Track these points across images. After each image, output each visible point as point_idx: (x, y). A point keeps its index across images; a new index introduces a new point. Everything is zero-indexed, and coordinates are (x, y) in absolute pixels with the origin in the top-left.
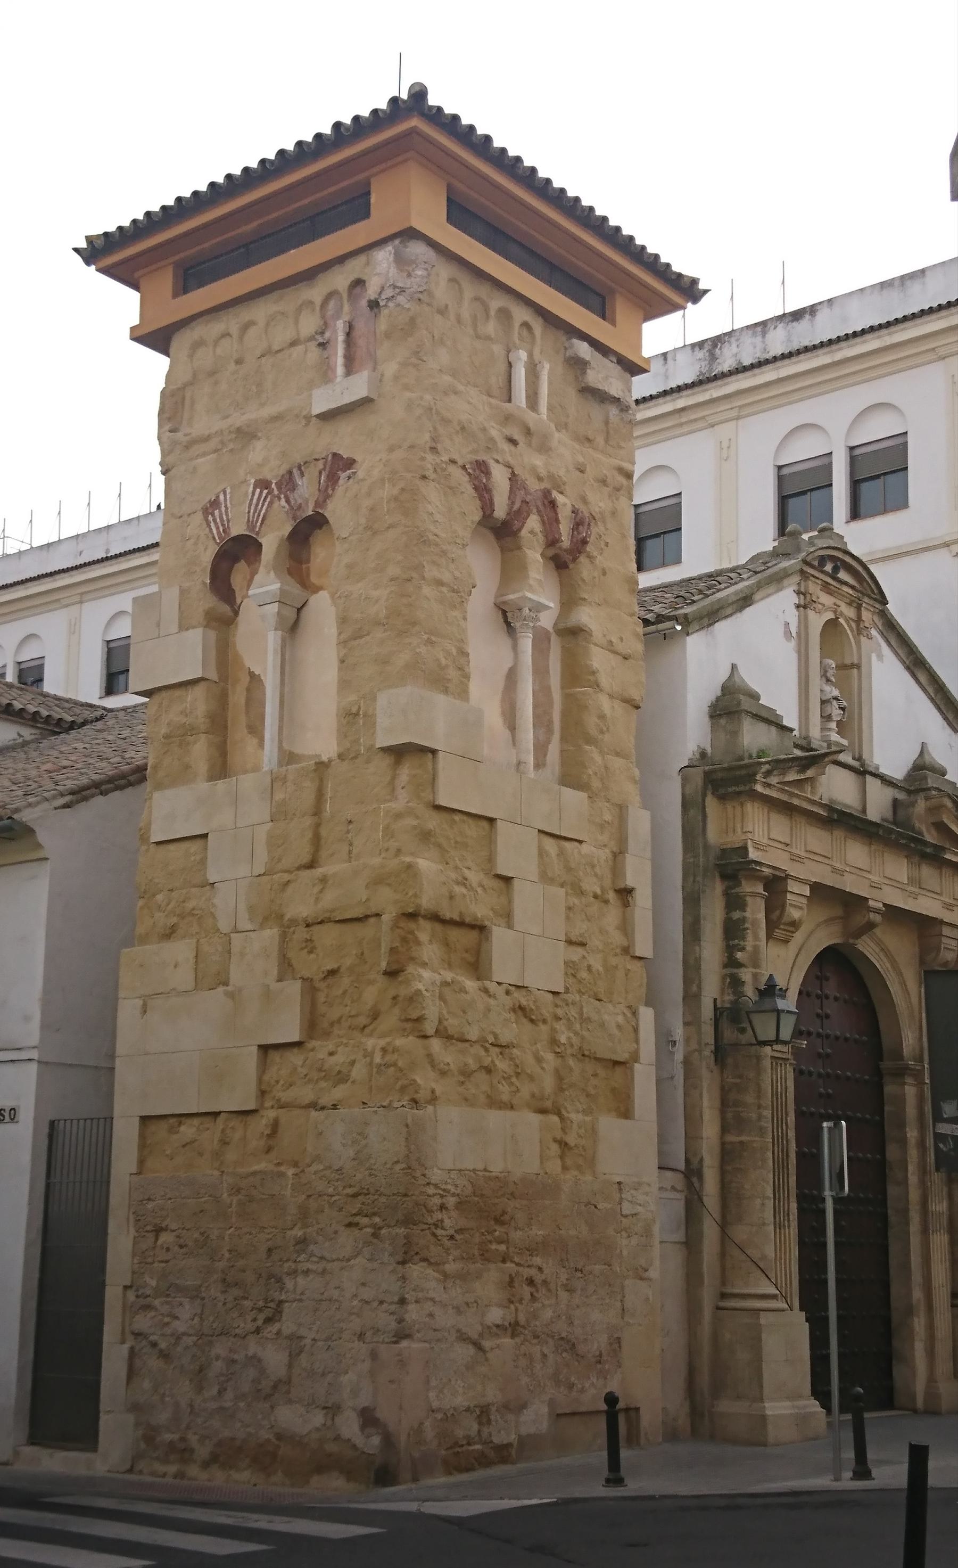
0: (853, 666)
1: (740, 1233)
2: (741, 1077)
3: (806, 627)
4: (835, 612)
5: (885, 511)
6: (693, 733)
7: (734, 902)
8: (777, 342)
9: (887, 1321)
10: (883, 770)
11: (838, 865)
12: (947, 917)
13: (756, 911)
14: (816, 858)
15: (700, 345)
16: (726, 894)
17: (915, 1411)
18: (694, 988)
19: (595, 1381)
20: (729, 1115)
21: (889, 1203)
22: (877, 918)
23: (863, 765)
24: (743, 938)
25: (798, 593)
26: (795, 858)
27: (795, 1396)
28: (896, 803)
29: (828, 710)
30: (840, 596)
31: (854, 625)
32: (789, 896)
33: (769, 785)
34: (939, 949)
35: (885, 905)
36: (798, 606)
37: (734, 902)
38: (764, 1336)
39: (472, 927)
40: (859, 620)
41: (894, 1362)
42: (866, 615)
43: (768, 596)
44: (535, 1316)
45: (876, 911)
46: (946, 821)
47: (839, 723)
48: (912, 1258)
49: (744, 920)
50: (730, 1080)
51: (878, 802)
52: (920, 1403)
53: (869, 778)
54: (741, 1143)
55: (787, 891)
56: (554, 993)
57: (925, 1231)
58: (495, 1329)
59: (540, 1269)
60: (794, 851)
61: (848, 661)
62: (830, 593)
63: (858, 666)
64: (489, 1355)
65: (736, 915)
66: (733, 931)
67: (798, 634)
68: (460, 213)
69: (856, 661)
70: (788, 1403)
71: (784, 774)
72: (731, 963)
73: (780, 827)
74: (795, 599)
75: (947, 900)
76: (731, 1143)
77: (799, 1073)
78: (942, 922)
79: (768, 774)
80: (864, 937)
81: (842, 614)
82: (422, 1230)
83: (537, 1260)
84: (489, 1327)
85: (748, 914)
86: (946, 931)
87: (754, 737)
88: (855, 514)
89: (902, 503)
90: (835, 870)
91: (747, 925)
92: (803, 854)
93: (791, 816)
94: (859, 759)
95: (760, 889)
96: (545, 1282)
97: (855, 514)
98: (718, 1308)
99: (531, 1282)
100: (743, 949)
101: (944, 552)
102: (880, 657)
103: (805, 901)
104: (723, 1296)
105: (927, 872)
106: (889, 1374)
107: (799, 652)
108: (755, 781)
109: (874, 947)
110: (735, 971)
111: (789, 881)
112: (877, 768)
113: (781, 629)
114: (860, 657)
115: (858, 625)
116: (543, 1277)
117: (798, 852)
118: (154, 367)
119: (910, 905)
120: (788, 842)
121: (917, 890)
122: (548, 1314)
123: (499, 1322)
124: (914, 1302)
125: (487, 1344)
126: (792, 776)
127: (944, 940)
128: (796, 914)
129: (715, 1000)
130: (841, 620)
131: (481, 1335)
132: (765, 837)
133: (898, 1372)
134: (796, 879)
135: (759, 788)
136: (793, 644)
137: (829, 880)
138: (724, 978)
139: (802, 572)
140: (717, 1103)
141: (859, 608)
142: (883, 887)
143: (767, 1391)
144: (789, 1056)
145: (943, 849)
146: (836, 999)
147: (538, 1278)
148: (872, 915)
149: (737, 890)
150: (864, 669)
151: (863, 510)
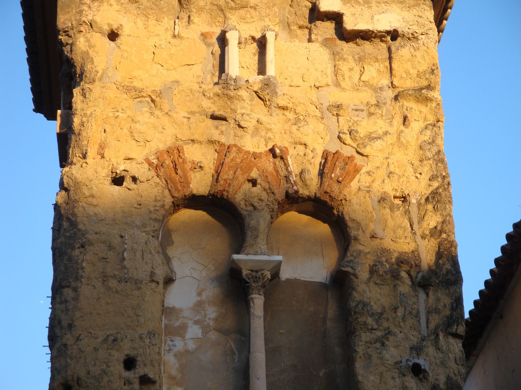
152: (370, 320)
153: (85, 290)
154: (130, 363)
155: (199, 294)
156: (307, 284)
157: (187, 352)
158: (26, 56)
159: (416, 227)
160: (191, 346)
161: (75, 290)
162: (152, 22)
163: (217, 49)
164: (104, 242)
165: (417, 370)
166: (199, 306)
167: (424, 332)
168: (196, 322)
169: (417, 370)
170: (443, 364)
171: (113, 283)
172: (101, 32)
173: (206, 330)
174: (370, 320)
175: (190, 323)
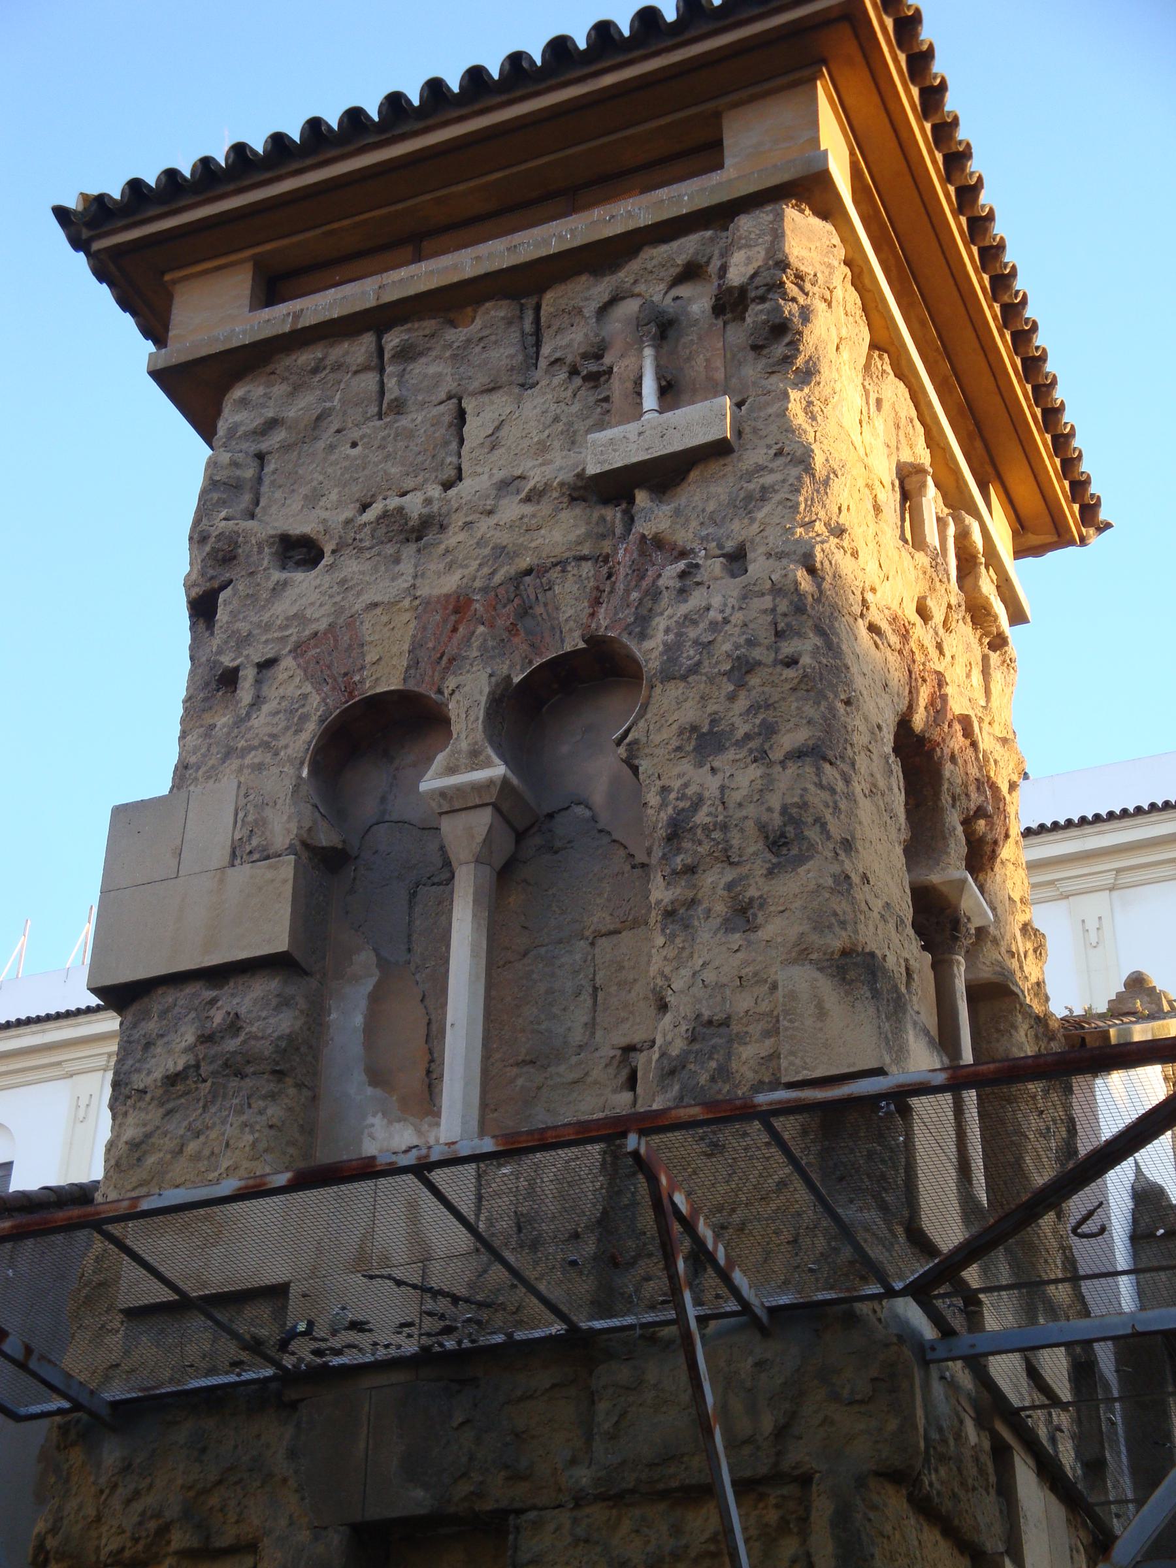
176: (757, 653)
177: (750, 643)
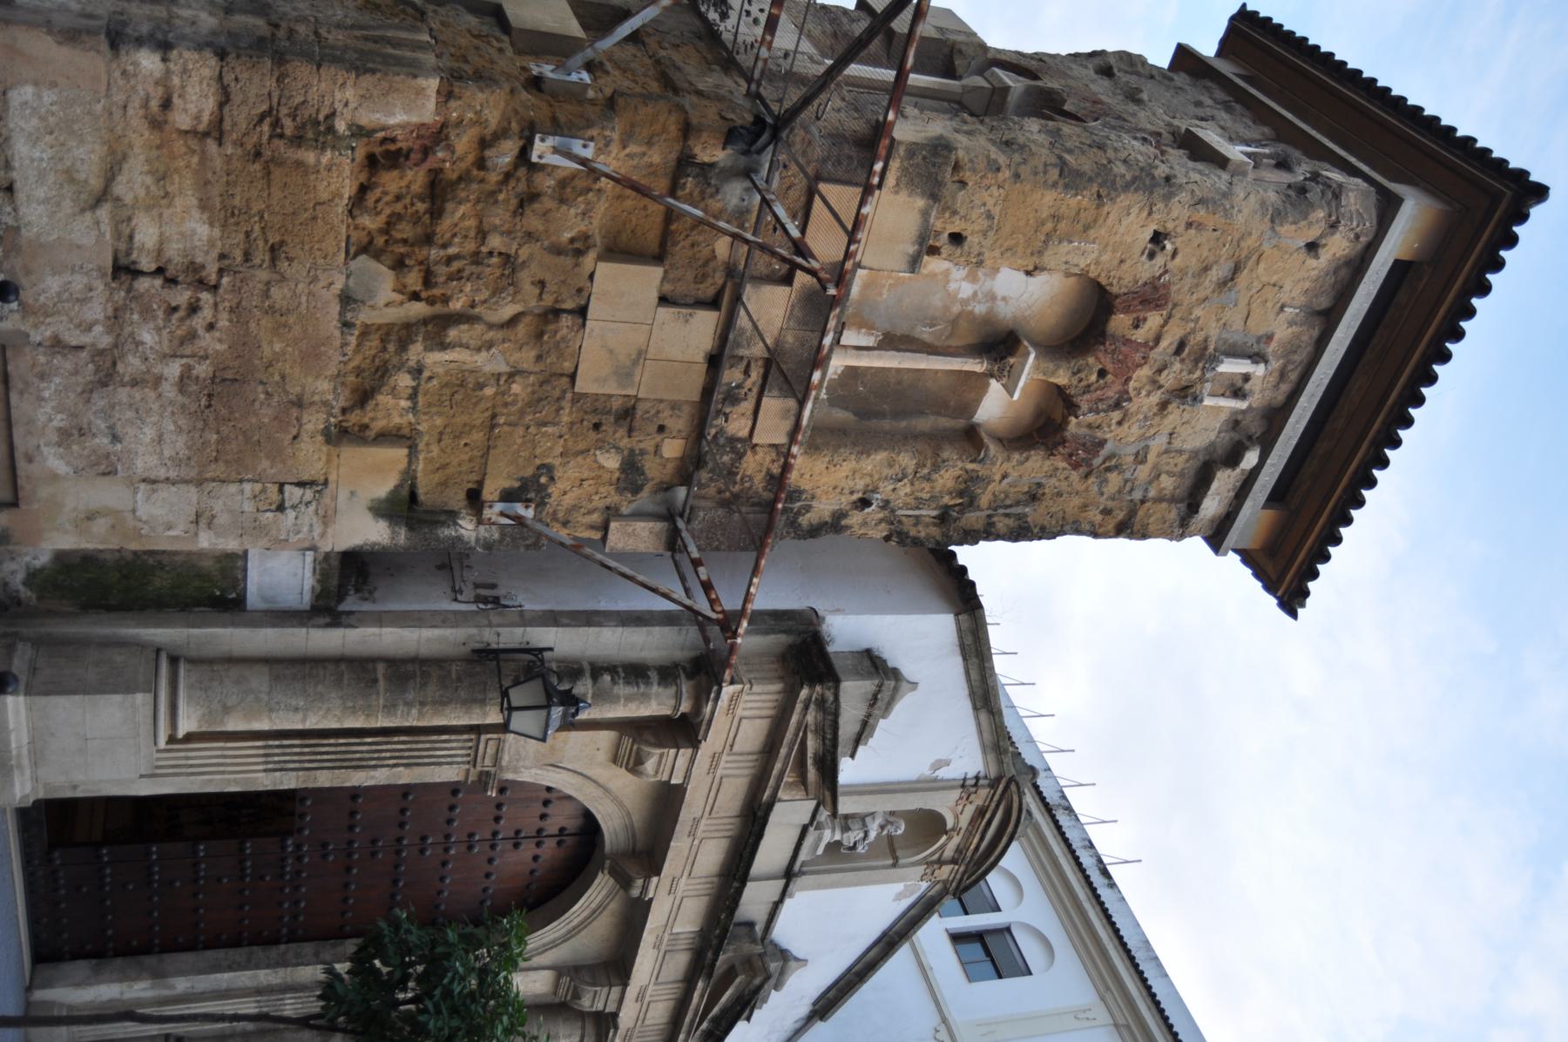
0: (896, 859)
1: (259, 680)
2: (459, 679)
3: (943, 788)
4: (953, 829)
5: (963, 964)
6: (847, 629)
7: (667, 674)
8: (1087, 860)
9: (146, 950)
10: (788, 902)
11: (702, 827)
12: (632, 991)
13: (657, 703)
14: (712, 794)
15: (1064, 797)
16: (676, 665)
17: (29, 989)
18: (566, 621)
19: (55, 423)
20: (410, 667)
21: (293, 946)
22: (635, 892)
23: (797, 875)
24: (628, 683)
25: (977, 778)
26: (715, 758)
27: (37, 756)
28: (750, 925)
29: (855, 825)
30: (970, 833)
31: (936, 857)
32: (673, 751)
33: (806, 708)
34: (595, 985)
35: (651, 900)
36: (965, 779)
37: (667, 674)
38: (117, 698)
39: (663, 244)
40: (941, 863)
41: (94, 962)
42: (947, 869)
43: (980, 732)
44: (147, 313)
45: (645, 888)
46: (738, 980)
47: (838, 844)
48: (226, 975)
49: (648, 683)
50: (454, 668)
51: (754, 901)
52: (39, 995)
53: (782, 882)
54: (376, 681)
55: (678, 748)
56: (573, 377)
57: (259, 991)
58: (127, 232)
59: (211, 327)
60: (724, 758)
61: (899, 853)
62: (973, 821)
63: (894, 865)
64: (88, 215)
65: (653, 675)
66: (635, 672)
67: (935, 780)
68: (1400, 269)
69: (901, 861)
70: (25, 740)
71: (816, 731)
72: (598, 670)
73: (752, 734)
74: (971, 774)
75: (649, 992)
76: (375, 670)
77: (454, 789)
78: (625, 985)
79: (821, 703)
80: (612, 881)
81: (950, 839)
82: (270, 94)
83: (223, 323)
84: (129, 219)
85: (655, 688)
86: (616, 991)
87: (853, 693)
88: (957, 938)
89: (971, 978)
90: (697, 822)
91: (642, 687)
92: (719, 772)
93: (761, 752)
94: (801, 873)
95: (685, 707)
96: (192, 336)
97: (957, 938)
98: (158, 651)
99: (194, 309)
100: (614, 682)
101: (937, 1019)
102: (899, 897)
103: (665, 778)
104: (174, 660)
105: (680, 962)
106: (75, 956)
107: (918, 781)
108: (812, 686)
109: (597, 901)
110: (588, 675)
111: (690, 751)
112: (791, 896)
113: (943, 757)
114: (904, 866)
115: (933, 863)
116: (201, 332)
117: (722, 764)
118: (1161, 58)
119: (648, 938)
120: (736, 749)
121: (663, 948)
122: (147, 337)
123: (137, 238)
124: (172, 981)
125: (104, 213)
126: (812, 744)
127: (606, 990)
128: (649, 766)
129: (551, 649)
130: (944, 838)
131: (118, 199)
132: (741, 713)
133: (81, 968)
134: (692, 761)
135: (804, 693)
136: (927, 772)
137: (686, 815)
138: (577, 661)
139: (998, 779)
140: (424, 651)
141: (954, 861)
142: (671, 897)
143: (41, 701)
144: (479, 768)
145: (710, 976)
146: (536, 858)
147: (198, 322)
148: (640, 882)
149: (683, 676)
150: (893, 871)
151: (960, 947)
152: (926, 471)
153: (1050, 197)
154: (957, 238)
155: (1004, 299)
156: (978, 401)
157: (948, 282)
158: (1249, 571)
159: (1001, 511)
160: (952, 286)
161: (1055, 185)
162: (1307, 285)
163: (1251, 351)
164: (1095, 221)
165: (864, 503)
166: (992, 297)
167: (899, 512)
168: (975, 294)
169: (864, 503)
170: (864, 524)
171: (1049, 226)
172: (1321, 236)
173: (965, 302)
174: (926, 471)
175: (976, 287)
176: (1110, 154)
177: (1116, 150)
